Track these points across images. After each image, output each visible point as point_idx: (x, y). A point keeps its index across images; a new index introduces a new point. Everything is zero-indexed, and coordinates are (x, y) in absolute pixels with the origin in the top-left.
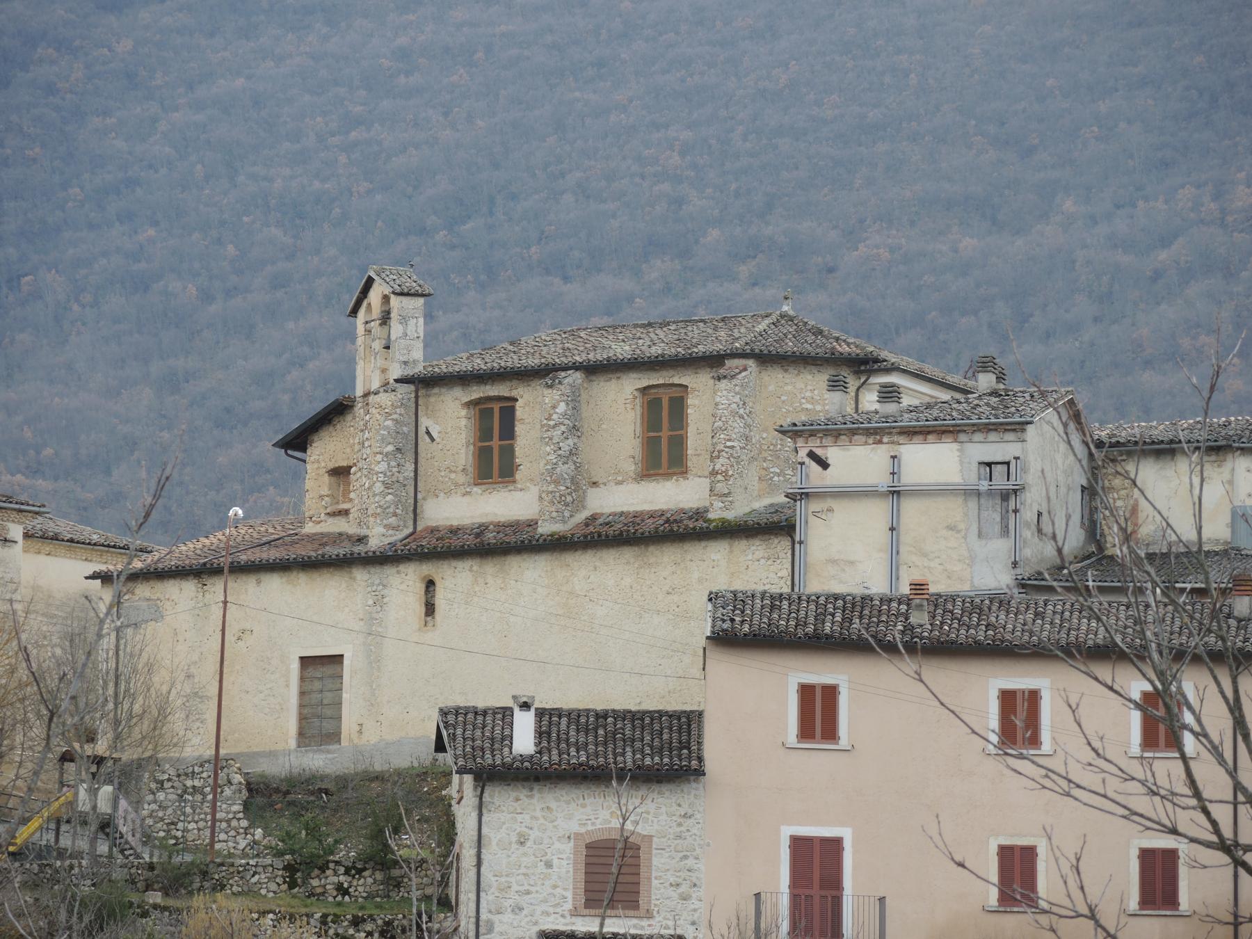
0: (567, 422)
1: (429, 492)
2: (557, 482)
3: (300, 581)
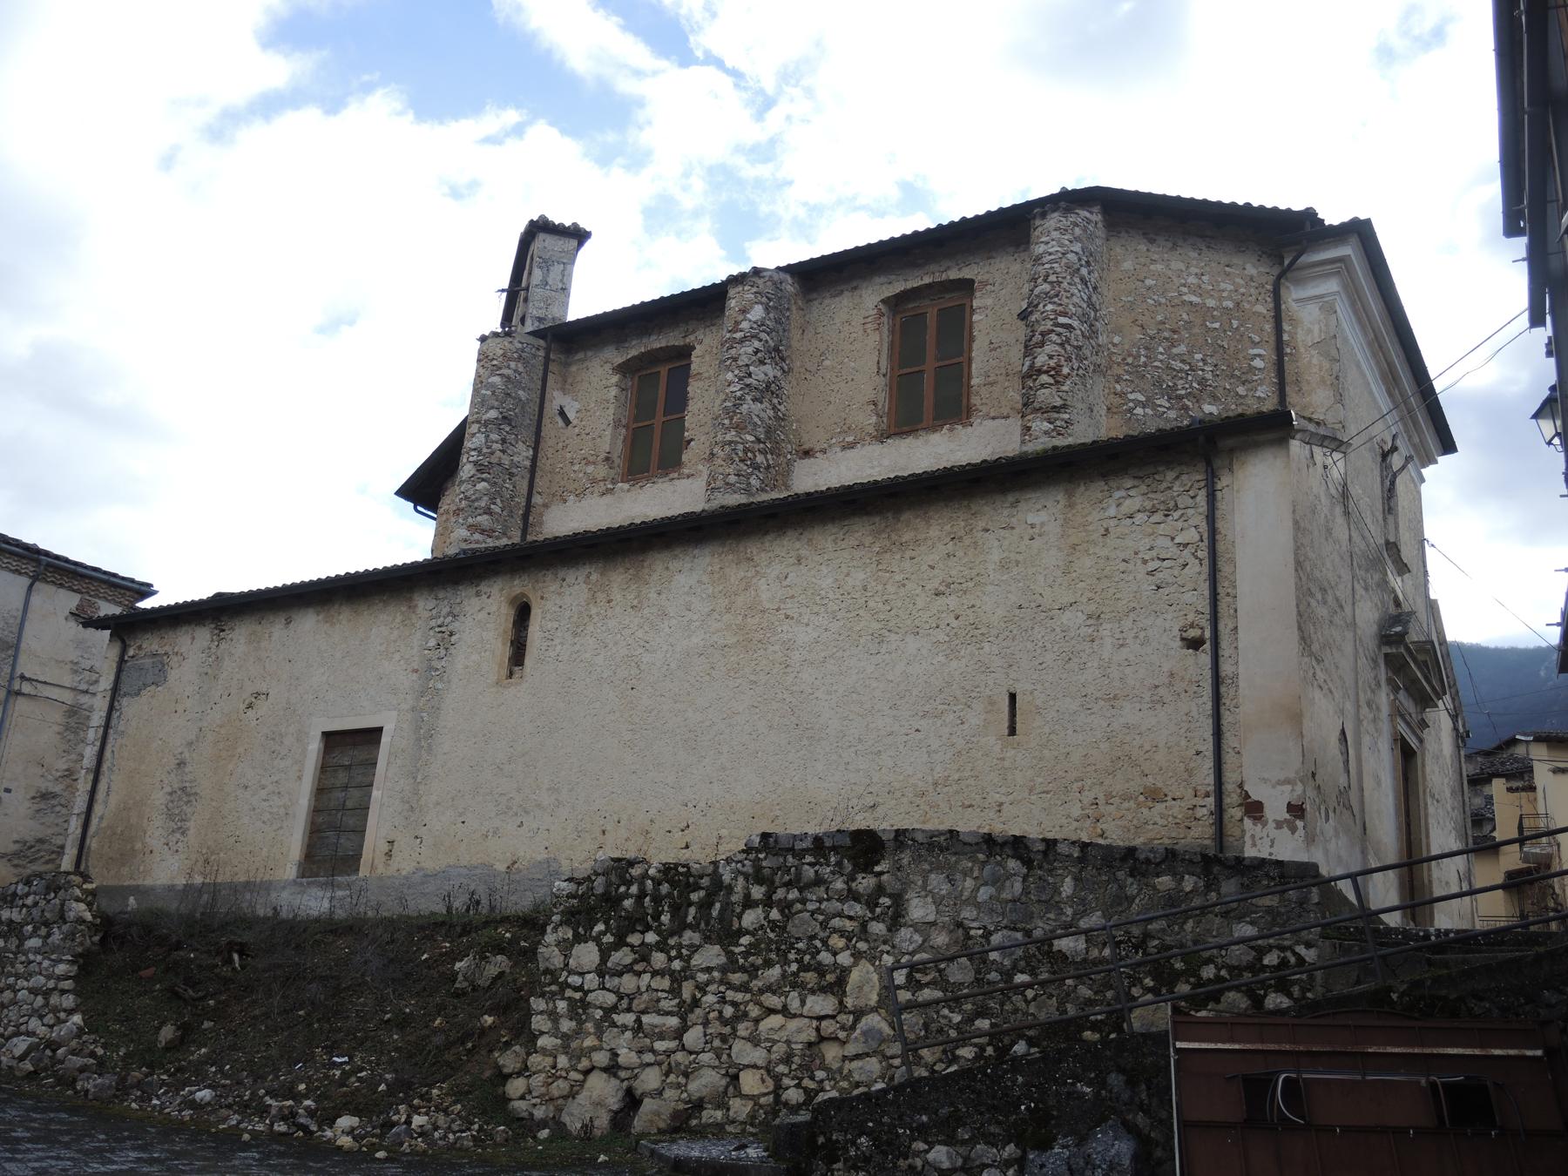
0: (763, 336)
1: (554, 495)
2: (739, 428)
3: (341, 617)
